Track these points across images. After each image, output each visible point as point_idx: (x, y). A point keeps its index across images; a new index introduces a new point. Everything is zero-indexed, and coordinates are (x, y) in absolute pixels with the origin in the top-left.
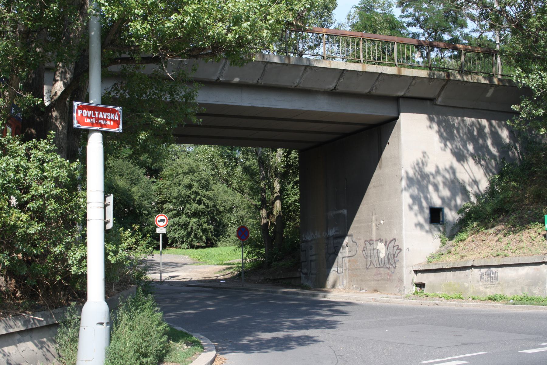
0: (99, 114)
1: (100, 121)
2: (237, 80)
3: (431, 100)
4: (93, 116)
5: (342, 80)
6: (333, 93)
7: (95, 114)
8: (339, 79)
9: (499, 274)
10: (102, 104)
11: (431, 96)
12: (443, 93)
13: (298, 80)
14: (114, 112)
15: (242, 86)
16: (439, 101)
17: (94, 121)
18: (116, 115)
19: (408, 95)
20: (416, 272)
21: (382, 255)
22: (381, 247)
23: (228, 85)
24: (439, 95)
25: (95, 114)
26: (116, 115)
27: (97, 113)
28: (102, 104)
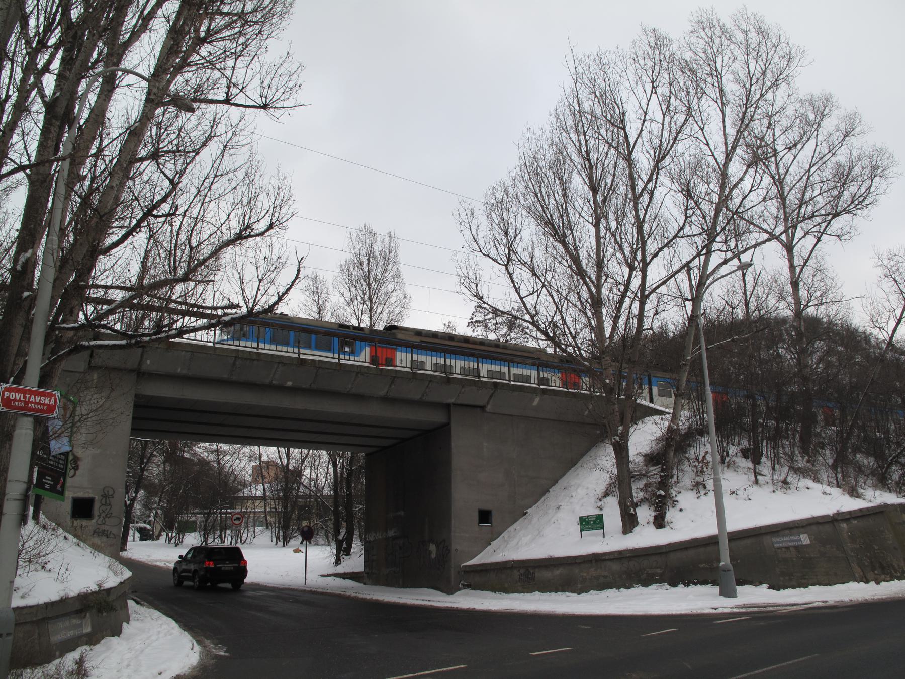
0: (30, 398)
1: (30, 405)
2: (289, 384)
3: (482, 408)
4: (22, 399)
5: (393, 387)
6: (387, 400)
7: (25, 397)
8: (390, 386)
9: (536, 575)
10: (39, 387)
11: (481, 404)
12: (491, 401)
13: (350, 386)
14: (50, 396)
15: (295, 390)
16: (489, 408)
17: (23, 405)
18: (53, 400)
19: (459, 402)
20: (323, 576)
21: (433, 556)
22: (433, 548)
23: (280, 389)
24: (488, 403)
25: (25, 397)
26: (53, 400)
27: (28, 396)
28: (39, 387)
